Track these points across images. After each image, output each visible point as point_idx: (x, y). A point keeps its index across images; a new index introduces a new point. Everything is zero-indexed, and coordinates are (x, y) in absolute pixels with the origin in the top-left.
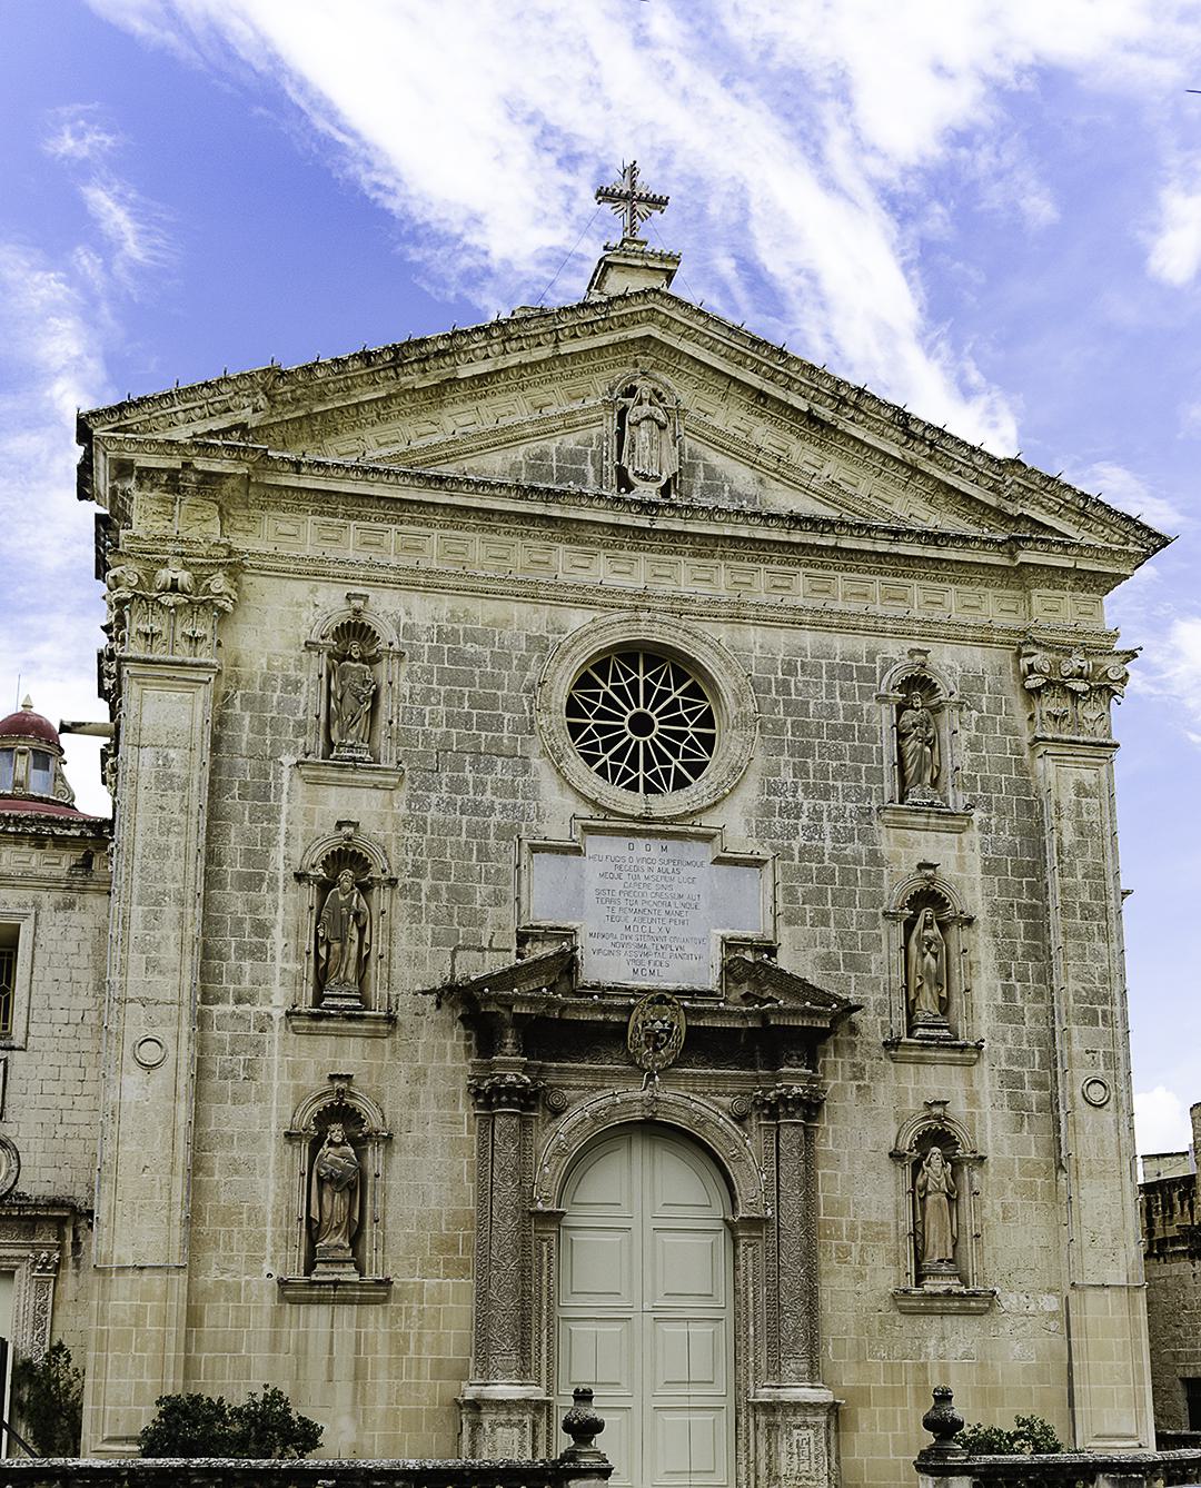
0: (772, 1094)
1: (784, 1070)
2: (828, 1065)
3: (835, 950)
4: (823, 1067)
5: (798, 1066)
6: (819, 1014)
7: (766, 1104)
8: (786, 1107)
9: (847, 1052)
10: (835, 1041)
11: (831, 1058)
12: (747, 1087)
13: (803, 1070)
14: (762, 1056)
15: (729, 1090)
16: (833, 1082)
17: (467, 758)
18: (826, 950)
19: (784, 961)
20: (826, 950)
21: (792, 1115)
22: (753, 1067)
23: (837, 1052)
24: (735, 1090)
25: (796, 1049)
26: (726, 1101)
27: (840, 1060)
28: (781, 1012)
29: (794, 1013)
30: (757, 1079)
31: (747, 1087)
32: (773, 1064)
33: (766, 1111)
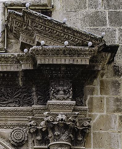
0: (43, 123)
1: (53, 101)
2: (95, 101)
3: (102, 9)
4: (91, 103)
5: (64, 99)
6: (78, 53)
7: (37, 132)
8: (53, 131)
9: (111, 90)
10: (102, 83)
11: (97, 95)
12: (24, 120)
13: (69, 102)
14: (37, 94)
15: (9, 123)
16: (99, 114)
17: (36, 81)
18: (93, 10)
19: (58, 16)
20: (93, 10)
21: (58, 137)
22: (30, 104)
23: (103, 89)
24: (14, 123)
25: (63, 86)
26: (6, 132)
27: (106, 96)
28: (45, 53)
29: (57, 53)
30: (32, 112)
31: (24, 120)
32: (44, 98)
33: (39, 138)
